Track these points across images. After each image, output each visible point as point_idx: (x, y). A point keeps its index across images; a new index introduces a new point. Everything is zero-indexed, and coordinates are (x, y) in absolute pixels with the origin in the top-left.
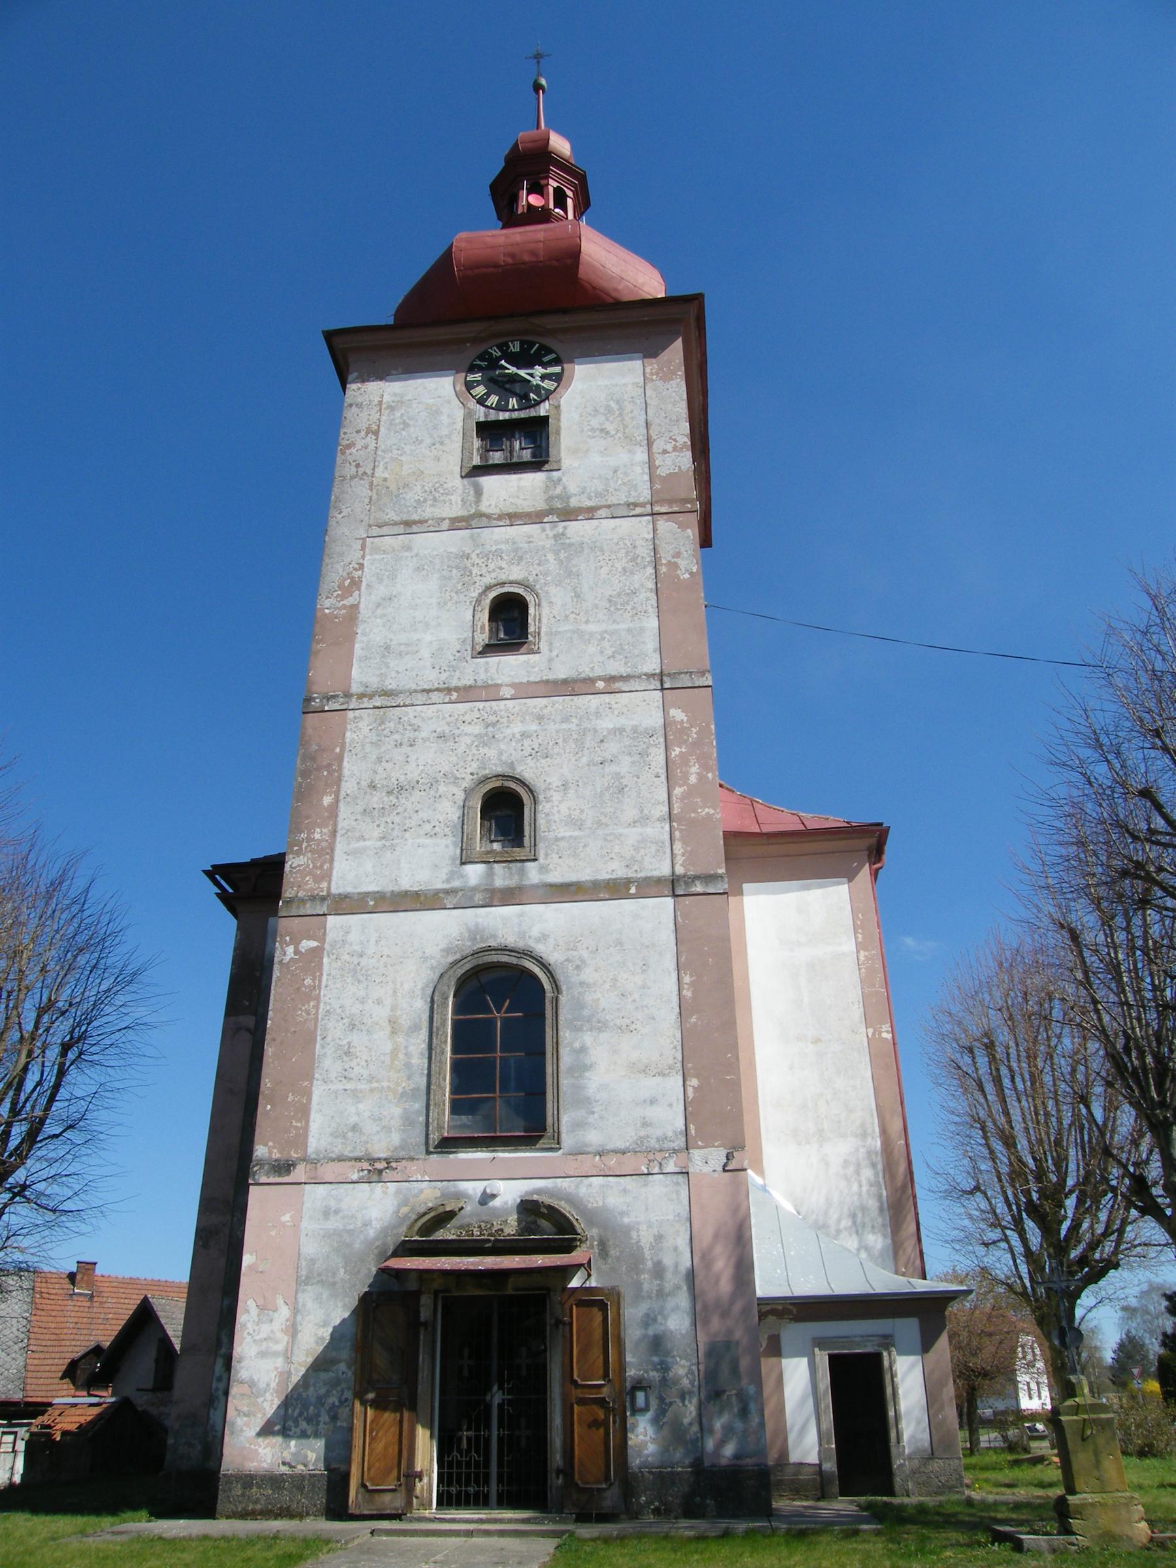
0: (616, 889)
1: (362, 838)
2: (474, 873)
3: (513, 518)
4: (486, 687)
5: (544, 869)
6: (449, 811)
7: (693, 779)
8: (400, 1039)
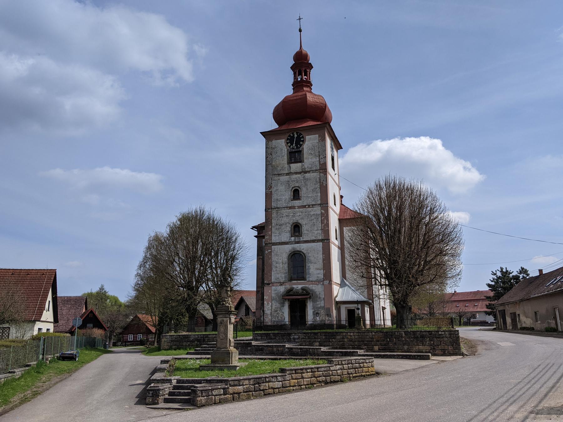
0: (313, 241)
2: (293, 238)
3: (296, 173)
6: (289, 229)
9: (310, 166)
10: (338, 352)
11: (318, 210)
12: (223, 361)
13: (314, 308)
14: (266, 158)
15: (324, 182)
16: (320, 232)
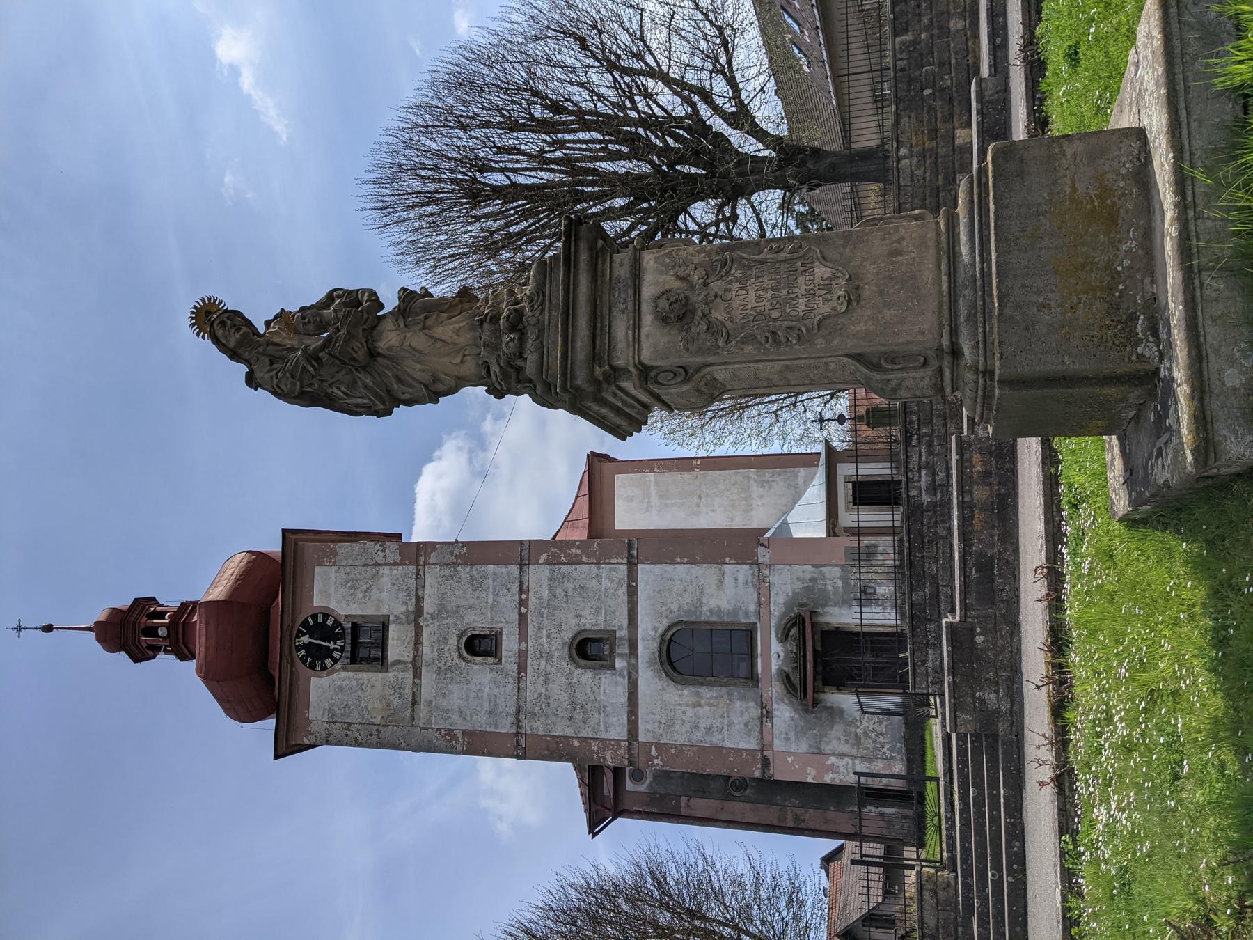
0: (632, 592)
1: (598, 724)
2: (620, 664)
3: (417, 642)
4: (519, 657)
5: (621, 628)
7: (579, 552)
8: (703, 702)
9: (402, 596)
11: (538, 575)
13: (845, 602)
14: (357, 743)
15: (457, 551)
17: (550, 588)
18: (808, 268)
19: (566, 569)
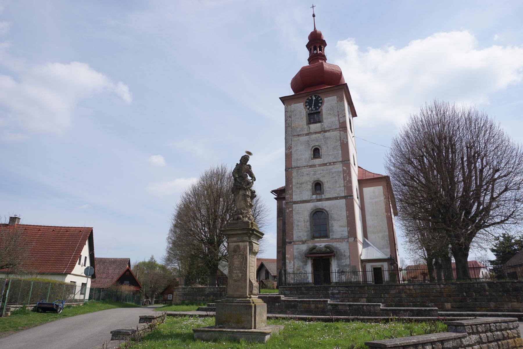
0: (336, 198)
2: (314, 196)
3: (316, 133)
9: (330, 125)
10: (407, 310)
11: (339, 167)
12: (239, 323)
13: (339, 266)
14: (286, 121)
15: (345, 140)
16: (343, 188)
17: (335, 172)
18: (241, 273)
19: (342, 176)
